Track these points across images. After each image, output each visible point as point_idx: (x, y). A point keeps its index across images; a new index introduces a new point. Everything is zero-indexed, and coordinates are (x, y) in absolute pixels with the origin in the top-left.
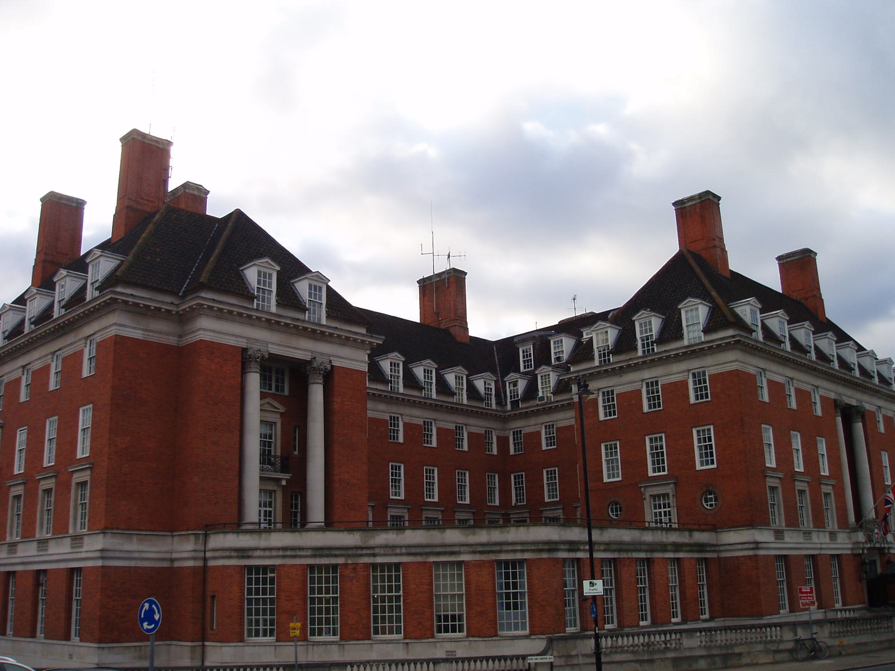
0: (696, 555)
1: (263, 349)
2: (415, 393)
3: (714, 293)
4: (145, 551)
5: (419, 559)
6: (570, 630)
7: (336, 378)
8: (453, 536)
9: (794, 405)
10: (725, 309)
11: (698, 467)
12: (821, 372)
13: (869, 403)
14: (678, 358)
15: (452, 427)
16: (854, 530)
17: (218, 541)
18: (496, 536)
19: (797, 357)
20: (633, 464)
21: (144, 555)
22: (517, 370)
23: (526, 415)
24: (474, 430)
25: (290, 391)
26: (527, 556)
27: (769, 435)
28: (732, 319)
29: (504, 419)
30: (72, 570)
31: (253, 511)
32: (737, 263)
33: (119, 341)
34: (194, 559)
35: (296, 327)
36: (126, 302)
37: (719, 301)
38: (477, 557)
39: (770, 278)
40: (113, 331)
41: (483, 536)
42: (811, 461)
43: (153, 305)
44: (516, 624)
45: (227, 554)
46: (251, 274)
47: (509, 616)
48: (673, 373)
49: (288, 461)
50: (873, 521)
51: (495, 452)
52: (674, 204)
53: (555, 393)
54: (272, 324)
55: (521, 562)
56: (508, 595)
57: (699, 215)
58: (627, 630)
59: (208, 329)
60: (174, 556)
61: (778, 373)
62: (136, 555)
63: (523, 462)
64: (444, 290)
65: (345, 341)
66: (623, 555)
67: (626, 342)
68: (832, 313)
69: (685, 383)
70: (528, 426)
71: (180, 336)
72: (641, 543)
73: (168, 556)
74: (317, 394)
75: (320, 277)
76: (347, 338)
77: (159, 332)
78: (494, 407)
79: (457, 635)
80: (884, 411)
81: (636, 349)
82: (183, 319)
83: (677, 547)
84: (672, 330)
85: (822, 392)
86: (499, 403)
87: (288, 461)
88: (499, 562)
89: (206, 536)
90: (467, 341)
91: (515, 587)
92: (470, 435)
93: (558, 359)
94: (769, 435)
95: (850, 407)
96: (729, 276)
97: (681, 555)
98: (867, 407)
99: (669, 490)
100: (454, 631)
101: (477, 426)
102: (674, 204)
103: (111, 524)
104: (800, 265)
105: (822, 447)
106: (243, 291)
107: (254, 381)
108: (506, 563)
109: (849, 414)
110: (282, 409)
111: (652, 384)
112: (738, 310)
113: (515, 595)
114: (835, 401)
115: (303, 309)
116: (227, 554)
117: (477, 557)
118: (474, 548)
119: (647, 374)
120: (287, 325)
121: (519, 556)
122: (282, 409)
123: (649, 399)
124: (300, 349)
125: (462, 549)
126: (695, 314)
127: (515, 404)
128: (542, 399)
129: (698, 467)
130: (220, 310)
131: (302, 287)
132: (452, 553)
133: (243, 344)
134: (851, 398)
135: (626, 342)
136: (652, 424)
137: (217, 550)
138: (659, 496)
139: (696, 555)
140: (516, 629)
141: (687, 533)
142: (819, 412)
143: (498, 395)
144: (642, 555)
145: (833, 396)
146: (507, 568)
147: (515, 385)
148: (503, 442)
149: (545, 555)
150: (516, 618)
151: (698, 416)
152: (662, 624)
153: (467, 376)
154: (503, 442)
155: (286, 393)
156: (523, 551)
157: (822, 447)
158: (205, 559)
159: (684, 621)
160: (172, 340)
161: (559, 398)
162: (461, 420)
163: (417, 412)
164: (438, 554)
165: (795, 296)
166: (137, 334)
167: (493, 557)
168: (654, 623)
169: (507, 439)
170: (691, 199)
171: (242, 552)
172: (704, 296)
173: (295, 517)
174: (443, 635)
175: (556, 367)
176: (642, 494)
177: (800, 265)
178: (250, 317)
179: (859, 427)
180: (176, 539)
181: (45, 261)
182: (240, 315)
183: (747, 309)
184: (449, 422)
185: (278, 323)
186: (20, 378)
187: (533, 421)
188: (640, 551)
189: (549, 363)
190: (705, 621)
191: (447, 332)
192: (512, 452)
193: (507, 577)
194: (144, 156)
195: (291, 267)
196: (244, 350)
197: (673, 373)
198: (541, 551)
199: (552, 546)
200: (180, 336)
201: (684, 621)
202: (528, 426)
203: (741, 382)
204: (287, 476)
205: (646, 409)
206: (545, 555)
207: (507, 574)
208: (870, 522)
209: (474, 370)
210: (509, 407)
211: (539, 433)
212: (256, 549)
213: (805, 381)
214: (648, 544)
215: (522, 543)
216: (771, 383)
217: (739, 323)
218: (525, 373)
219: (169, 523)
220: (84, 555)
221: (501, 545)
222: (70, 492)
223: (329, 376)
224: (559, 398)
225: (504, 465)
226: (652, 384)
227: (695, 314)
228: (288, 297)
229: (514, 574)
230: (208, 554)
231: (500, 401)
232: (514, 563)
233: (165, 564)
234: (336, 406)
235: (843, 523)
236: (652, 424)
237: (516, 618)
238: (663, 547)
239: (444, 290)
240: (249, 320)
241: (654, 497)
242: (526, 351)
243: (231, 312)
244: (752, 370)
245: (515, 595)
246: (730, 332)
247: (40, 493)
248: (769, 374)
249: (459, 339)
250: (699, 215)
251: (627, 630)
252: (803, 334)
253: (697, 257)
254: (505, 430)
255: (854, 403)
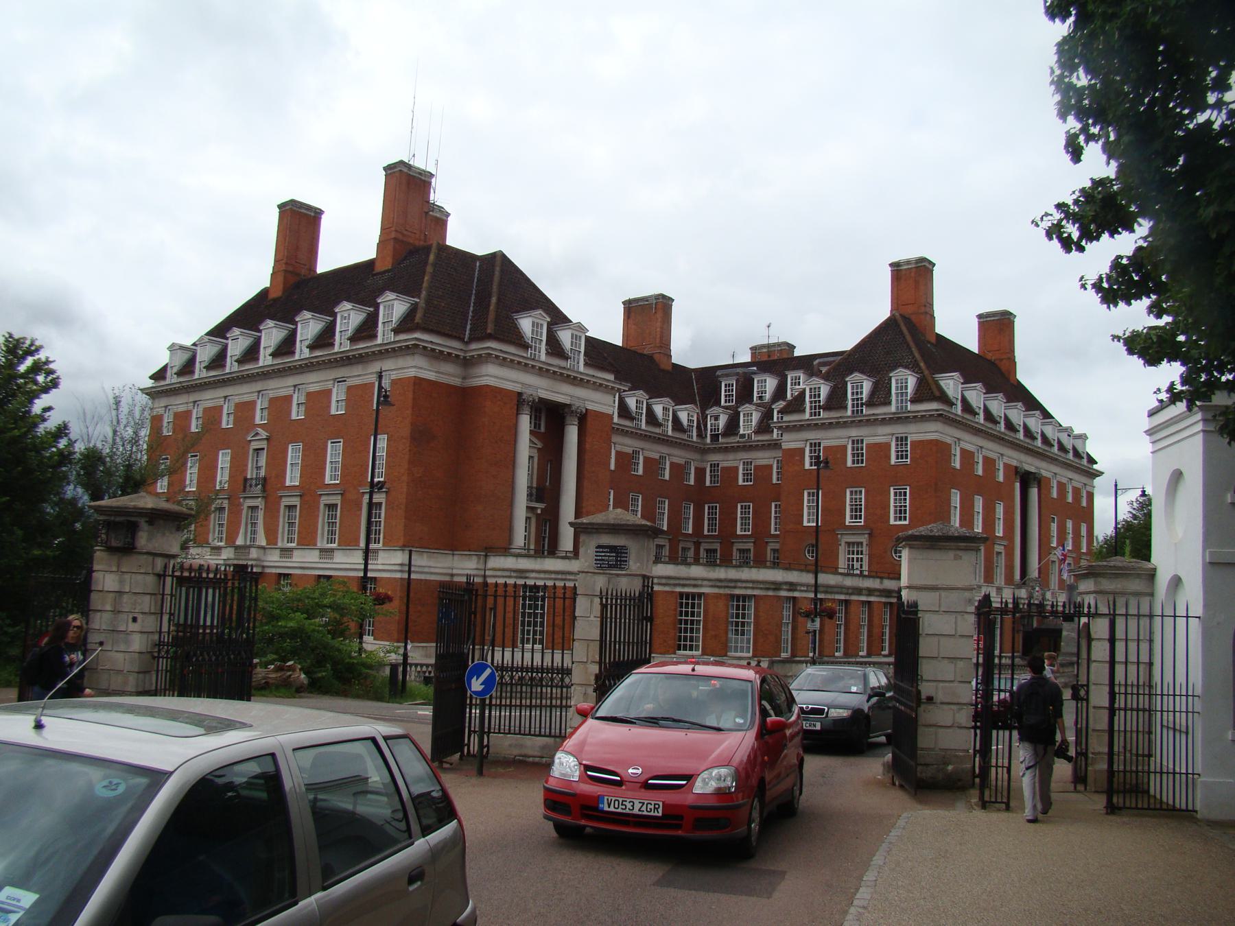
0: (883, 600)
1: (534, 394)
2: (627, 423)
3: (922, 364)
4: (437, 566)
5: (667, 589)
6: (784, 655)
7: (589, 419)
8: (697, 571)
9: (980, 472)
10: (930, 381)
11: (892, 522)
12: (1008, 441)
13: (1045, 469)
14: (884, 421)
15: (657, 456)
16: (1019, 587)
17: (496, 562)
18: (732, 574)
19: (989, 427)
20: (834, 512)
21: (432, 570)
22: (718, 403)
23: (726, 450)
24: (676, 460)
25: (546, 427)
26: (756, 592)
27: (956, 498)
28: (937, 394)
29: (704, 451)
30: (280, 574)
31: (519, 538)
32: (942, 328)
33: (418, 382)
34: (401, 571)
35: (562, 374)
36: (425, 348)
37: (926, 372)
38: (716, 591)
39: (969, 339)
40: (412, 373)
41: (721, 573)
42: (989, 522)
43: (446, 350)
44: (742, 648)
45: (507, 574)
46: (526, 324)
47: (736, 642)
48: (881, 435)
49: (546, 492)
50: (1035, 580)
51: (692, 482)
52: (891, 265)
53: (757, 432)
54: (542, 372)
55: (750, 597)
56: (737, 624)
57: (913, 279)
58: (826, 659)
59: (492, 376)
60: (455, 571)
61: (970, 442)
62: (426, 570)
63: (716, 495)
64: (650, 314)
65: (599, 387)
66: (829, 596)
67: (836, 400)
68: (1024, 376)
69: (888, 445)
70: (726, 460)
71: (464, 378)
72: (842, 587)
73: (450, 571)
74: (572, 434)
75: (581, 328)
76: (601, 385)
77: (447, 374)
78: (695, 439)
79: (694, 653)
80: (1059, 478)
81: (846, 408)
82: (468, 363)
83: (870, 592)
84: (880, 395)
85: (1006, 460)
86: (700, 435)
87: (546, 492)
88: (732, 596)
89: (486, 556)
90: (669, 368)
91: (743, 617)
92: (672, 464)
93: (760, 398)
94: (956, 498)
95: (1028, 473)
96: (933, 340)
97: (872, 599)
98: (1044, 473)
99: (864, 539)
100: (691, 649)
101: (679, 456)
102: (891, 265)
103: (410, 544)
104: (998, 326)
105: (1000, 510)
106: (517, 339)
107: (525, 423)
108: (738, 597)
109: (1027, 479)
110: (540, 445)
111: (857, 442)
112: (942, 383)
113: (743, 624)
114: (1016, 468)
115: (566, 358)
116: (507, 574)
117: (716, 591)
118: (717, 583)
119: (854, 432)
120: (555, 372)
121: (749, 592)
122: (540, 445)
123: (853, 455)
124: (561, 393)
125: (705, 583)
126: (905, 380)
127: (715, 437)
128: (743, 436)
129: (892, 522)
130: (504, 359)
131: (565, 337)
132: (695, 586)
133: (518, 388)
134: (1030, 464)
135: (836, 400)
136: (855, 478)
137: (499, 570)
138: (853, 543)
139: (883, 600)
140: (742, 651)
141: (878, 581)
142: (1001, 478)
143: (698, 427)
144: (842, 597)
145: (1015, 463)
146: (738, 601)
147: (717, 418)
148: (700, 473)
149: (770, 593)
150: (742, 641)
151: (896, 477)
152: (852, 656)
153: (549, 324)
154: (700, 473)
155: (543, 429)
156: (753, 588)
157: (1000, 510)
158: (485, 576)
159: (869, 655)
160: (457, 382)
161: (760, 438)
162: (665, 450)
163: (628, 441)
164: (684, 585)
165: (989, 356)
166: (431, 376)
167: (728, 591)
168: (846, 654)
169: (704, 470)
170: (908, 262)
171: (522, 573)
172: (914, 367)
173: (546, 543)
174: (682, 652)
175: (758, 405)
176: (838, 540)
177: (998, 326)
178: (526, 365)
179: (1034, 492)
180: (456, 558)
181: (286, 271)
182: (519, 363)
183: (951, 384)
184: (654, 451)
185: (548, 370)
186: (291, 396)
187: (731, 456)
188: (841, 593)
189: (750, 401)
190: (885, 656)
191: (650, 358)
192: (708, 484)
193: (738, 608)
194: (407, 187)
195: (558, 318)
196: (520, 394)
197: (881, 435)
198: (768, 589)
199: (777, 586)
200: (464, 378)
201: (869, 655)
202: (726, 460)
203: (940, 450)
204: (542, 506)
205: (849, 464)
206: (770, 593)
207: (738, 606)
208: (1033, 580)
209: (681, 399)
210: (708, 440)
211: (737, 468)
212: (533, 571)
213: (992, 449)
214: (848, 588)
215: (753, 582)
216: (963, 451)
217: (943, 398)
218: (726, 408)
219: (452, 543)
220: (380, 567)
221: (735, 582)
222: (361, 509)
223: (583, 418)
224: (760, 438)
225: (700, 495)
226: (857, 442)
227: (905, 380)
228: (555, 348)
229: (744, 606)
230: (488, 573)
231: (701, 435)
232: (745, 597)
233: (447, 579)
234: (588, 446)
235: (1009, 580)
236: (855, 478)
237: (742, 641)
238: (859, 591)
239: (650, 314)
240: (524, 367)
241: (848, 544)
242: (727, 388)
243: (512, 361)
244: (948, 440)
245: (692, 622)
246: (934, 406)
247: (322, 506)
248: (961, 442)
249: (662, 367)
250: (913, 279)
251: (826, 659)
252: (997, 406)
253: (906, 319)
254: (702, 461)
255: (1033, 470)
